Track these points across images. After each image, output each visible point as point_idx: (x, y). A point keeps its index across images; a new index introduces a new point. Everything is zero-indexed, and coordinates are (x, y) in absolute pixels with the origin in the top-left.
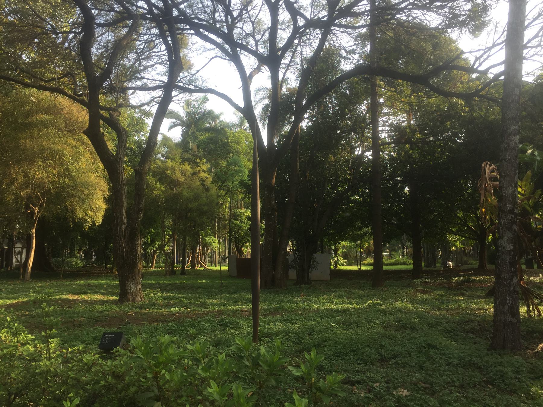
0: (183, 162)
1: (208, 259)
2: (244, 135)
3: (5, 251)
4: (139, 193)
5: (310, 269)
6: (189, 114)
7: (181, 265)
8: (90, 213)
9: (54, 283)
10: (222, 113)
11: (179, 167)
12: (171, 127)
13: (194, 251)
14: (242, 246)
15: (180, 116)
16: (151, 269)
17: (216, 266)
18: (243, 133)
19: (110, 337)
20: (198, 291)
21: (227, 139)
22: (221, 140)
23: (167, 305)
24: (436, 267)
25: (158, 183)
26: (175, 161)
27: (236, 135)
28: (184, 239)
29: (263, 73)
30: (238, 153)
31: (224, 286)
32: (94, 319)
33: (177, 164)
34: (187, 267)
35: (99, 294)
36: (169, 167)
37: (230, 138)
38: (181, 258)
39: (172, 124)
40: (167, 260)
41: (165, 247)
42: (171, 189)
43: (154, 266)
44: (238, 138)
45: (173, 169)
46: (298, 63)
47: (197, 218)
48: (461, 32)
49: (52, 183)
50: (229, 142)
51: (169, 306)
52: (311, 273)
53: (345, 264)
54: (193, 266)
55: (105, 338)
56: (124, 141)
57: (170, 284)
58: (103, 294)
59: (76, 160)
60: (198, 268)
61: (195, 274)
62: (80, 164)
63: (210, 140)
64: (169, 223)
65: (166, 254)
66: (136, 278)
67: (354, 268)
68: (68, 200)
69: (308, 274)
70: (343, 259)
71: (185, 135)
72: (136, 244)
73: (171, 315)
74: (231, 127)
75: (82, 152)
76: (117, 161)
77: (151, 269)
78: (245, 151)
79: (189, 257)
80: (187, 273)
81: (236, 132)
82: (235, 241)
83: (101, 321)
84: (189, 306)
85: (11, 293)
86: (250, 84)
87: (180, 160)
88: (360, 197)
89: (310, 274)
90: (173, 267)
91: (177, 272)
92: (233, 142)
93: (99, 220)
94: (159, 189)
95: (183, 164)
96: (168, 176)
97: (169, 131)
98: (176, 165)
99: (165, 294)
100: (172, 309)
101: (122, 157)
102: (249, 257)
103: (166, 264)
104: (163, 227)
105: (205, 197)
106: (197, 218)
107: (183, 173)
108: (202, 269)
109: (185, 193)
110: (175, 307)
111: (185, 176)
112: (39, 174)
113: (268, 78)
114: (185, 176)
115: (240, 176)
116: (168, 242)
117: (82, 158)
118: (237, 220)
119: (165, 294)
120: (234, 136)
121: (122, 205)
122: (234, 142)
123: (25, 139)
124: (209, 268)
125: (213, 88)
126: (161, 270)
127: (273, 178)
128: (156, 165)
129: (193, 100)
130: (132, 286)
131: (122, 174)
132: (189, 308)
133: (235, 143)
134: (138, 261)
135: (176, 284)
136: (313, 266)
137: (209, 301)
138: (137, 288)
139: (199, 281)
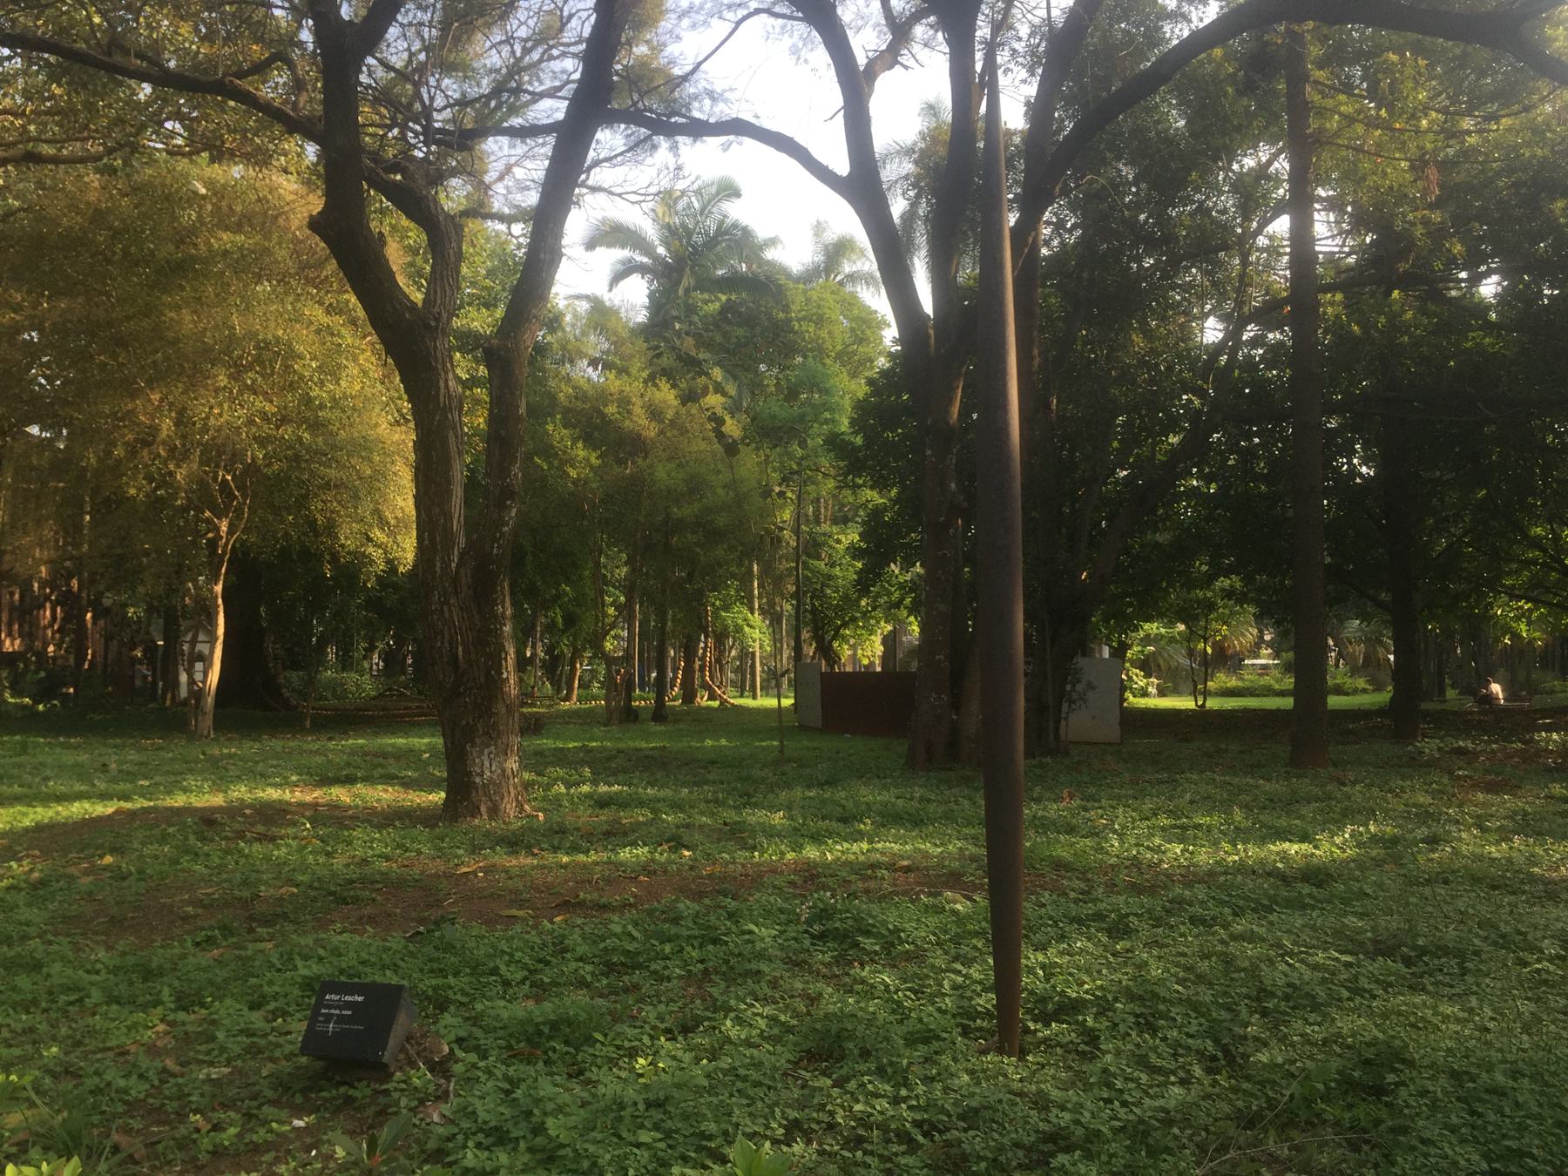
1: (731, 675)
2: (838, 298)
3: (160, 652)
4: (503, 433)
5: (1065, 706)
6: (671, 233)
7: (652, 695)
8: (378, 535)
9: (277, 744)
10: (772, 242)
11: (642, 396)
12: (617, 278)
13: (689, 652)
14: (834, 638)
15: (645, 239)
16: (566, 705)
18: (833, 293)
19: (348, 1005)
20: (710, 777)
21: (786, 309)
23: (608, 834)
26: (629, 374)
27: (815, 298)
28: (662, 620)
29: (906, 67)
30: (820, 351)
31: (789, 761)
32: (331, 893)
33: (638, 385)
34: (670, 700)
35: (393, 785)
36: (611, 395)
38: (654, 675)
39: (620, 267)
42: (621, 462)
43: (575, 698)
44: (819, 307)
45: (624, 402)
46: (1021, 34)
47: (698, 550)
49: (262, 442)
50: (790, 320)
51: (616, 835)
52: (1066, 719)
54: (689, 696)
55: (329, 1007)
56: (453, 259)
57: (620, 751)
58: (407, 784)
59: (330, 370)
60: (703, 700)
62: (343, 383)
66: (499, 735)
67: (1186, 703)
68: (316, 495)
69: (1058, 722)
70: (1145, 677)
71: (658, 305)
72: (496, 616)
73: (619, 876)
74: (810, 276)
75: (348, 345)
76: (427, 327)
77: (566, 705)
78: (839, 348)
79: (675, 671)
80: (671, 718)
82: (814, 621)
83: (356, 900)
84: (686, 840)
85: (130, 776)
86: (870, 96)
87: (645, 374)
88: (1208, 479)
89: (1063, 723)
90: (629, 699)
92: (804, 319)
93: (407, 550)
94: (582, 460)
95: (655, 385)
97: (611, 290)
99: (603, 789)
100: (625, 854)
101: (445, 315)
102: (879, 669)
104: (601, 582)
105: (724, 487)
106: (698, 550)
107: (655, 413)
108: (716, 704)
109: (661, 473)
110: (634, 844)
111: (661, 421)
112: (221, 415)
113: (918, 110)
114: (661, 421)
115: (826, 422)
116: (613, 626)
117: (351, 365)
118: (819, 558)
119: (603, 789)
120: (808, 300)
121: (449, 483)
123: (178, 308)
126: (597, 706)
127: (950, 401)
128: (574, 388)
129: (683, 192)
130: (487, 764)
131: (446, 373)
132: (688, 848)
133: (811, 321)
134: (505, 676)
135: (641, 749)
136: (1075, 696)
137: (755, 817)
138: (504, 771)
139: (709, 743)
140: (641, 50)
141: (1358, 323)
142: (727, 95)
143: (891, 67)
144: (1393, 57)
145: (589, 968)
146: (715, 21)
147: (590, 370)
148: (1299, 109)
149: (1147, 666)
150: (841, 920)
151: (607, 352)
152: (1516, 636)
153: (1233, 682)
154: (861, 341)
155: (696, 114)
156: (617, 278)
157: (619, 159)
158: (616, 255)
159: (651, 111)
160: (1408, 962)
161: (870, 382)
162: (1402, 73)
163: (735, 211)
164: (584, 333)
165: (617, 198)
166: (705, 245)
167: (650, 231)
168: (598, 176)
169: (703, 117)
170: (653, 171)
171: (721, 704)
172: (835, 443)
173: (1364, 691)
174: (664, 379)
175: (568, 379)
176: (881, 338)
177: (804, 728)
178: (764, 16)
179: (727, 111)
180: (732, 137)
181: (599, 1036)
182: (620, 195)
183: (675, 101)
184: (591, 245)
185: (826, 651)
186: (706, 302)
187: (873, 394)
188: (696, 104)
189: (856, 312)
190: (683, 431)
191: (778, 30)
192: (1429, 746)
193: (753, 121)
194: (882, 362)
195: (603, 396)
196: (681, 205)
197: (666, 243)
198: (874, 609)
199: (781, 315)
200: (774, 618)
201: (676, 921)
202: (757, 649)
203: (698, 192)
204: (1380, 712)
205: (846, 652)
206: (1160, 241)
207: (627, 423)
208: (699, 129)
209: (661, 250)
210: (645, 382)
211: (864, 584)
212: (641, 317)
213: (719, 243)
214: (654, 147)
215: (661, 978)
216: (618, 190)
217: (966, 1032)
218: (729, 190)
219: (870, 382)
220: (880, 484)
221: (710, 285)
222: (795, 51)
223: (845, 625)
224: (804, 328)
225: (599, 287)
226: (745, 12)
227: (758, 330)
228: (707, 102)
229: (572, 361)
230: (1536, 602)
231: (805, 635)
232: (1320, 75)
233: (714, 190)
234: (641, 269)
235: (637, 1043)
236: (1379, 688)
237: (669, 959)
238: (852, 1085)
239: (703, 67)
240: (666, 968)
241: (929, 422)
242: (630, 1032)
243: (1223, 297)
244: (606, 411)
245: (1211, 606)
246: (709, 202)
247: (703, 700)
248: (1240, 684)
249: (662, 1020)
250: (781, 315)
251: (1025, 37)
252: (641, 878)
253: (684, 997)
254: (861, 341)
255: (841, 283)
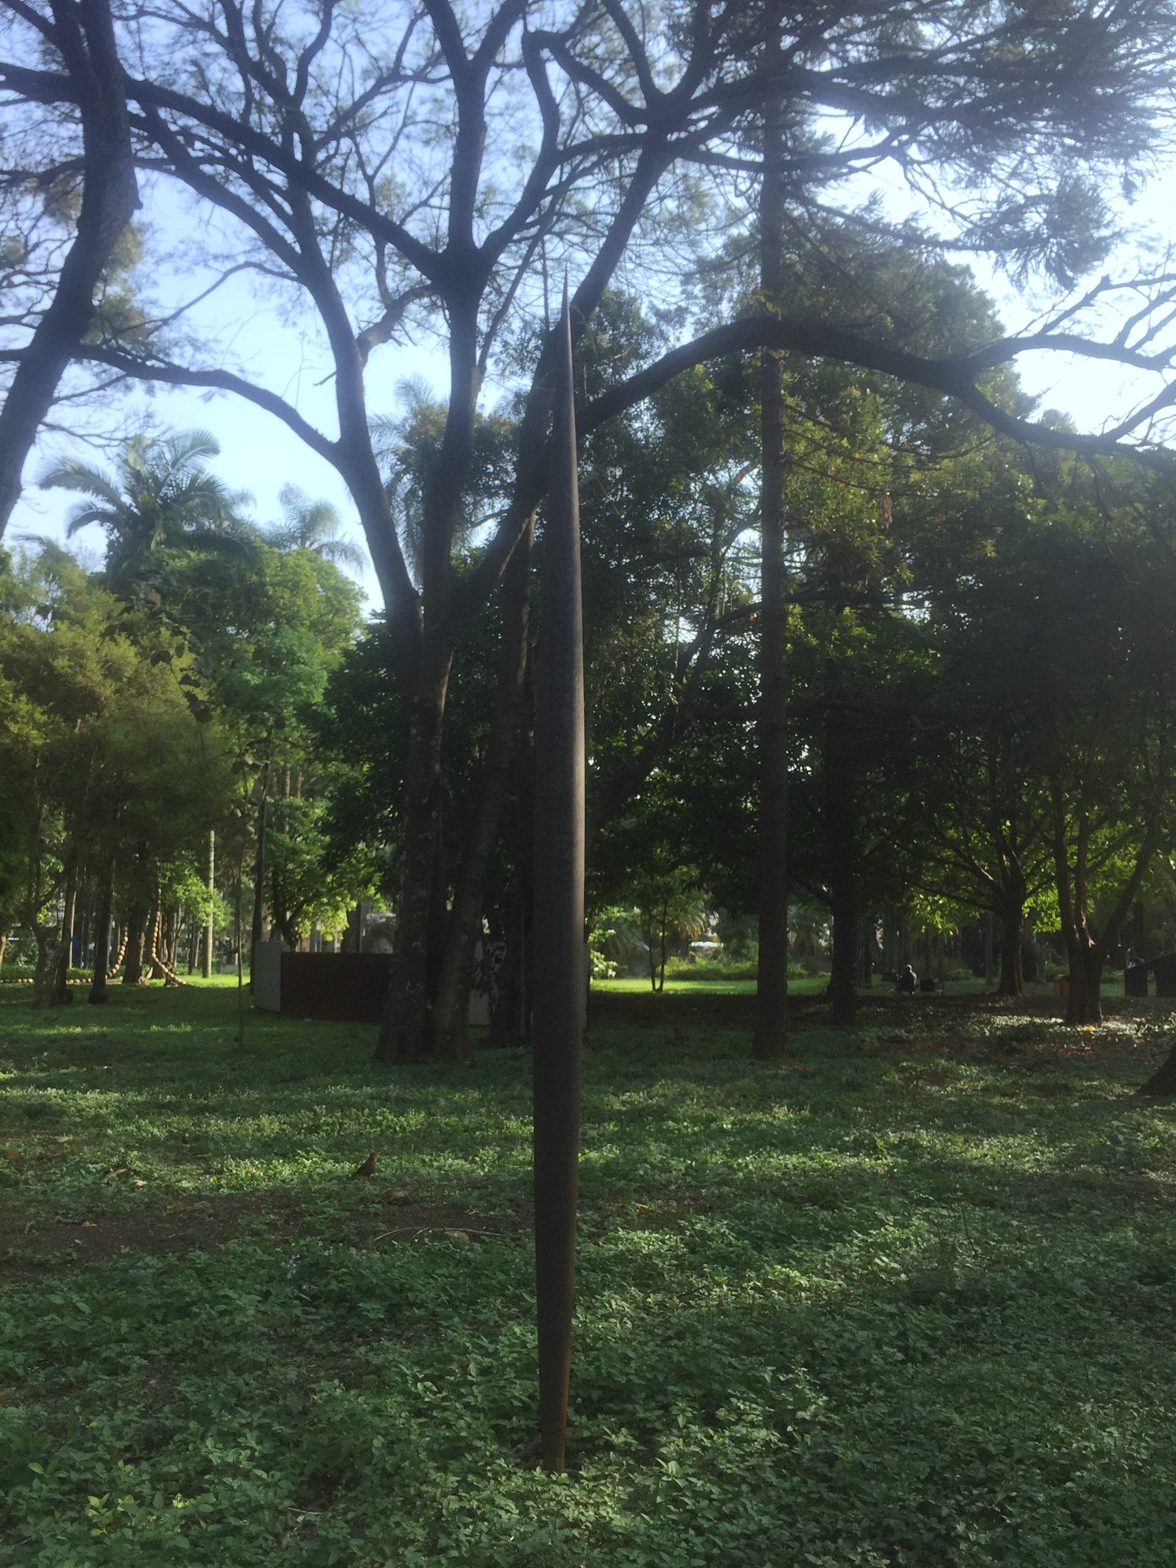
0: (109, 633)
2: (315, 566)
6: (139, 482)
10: (244, 498)
12: (76, 524)
15: (108, 485)
17: (205, 975)
21: (260, 573)
22: (242, 579)
24: (870, 987)
25: (23, 698)
27: (291, 564)
29: (400, 343)
30: (292, 619)
33: (94, 638)
37: (268, 571)
40: (43, 956)
41: (39, 910)
44: (295, 573)
48: (1024, 267)
50: (263, 584)
53: (611, 972)
60: (147, 979)
61: (138, 1002)
63: (200, 574)
64: (58, 833)
65: (44, 934)
67: (642, 985)
71: (117, 555)
74: (278, 541)
81: (289, 554)
82: (275, 896)
87: (102, 628)
90: (64, 976)
91: (78, 996)
92: (278, 584)
95: (115, 640)
96: (60, 675)
97: (69, 536)
98: (89, 641)
103: (41, 965)
107: (112, 670)
108: (160, 982)
116: (49, 897)
120: (283, 566)
122: (282, 584)
124: (184, 980)
125: (232, 370)
129: (154, 443)
140: (114, 290)
141: (815, 636)
142: (212, 345)
143: (384, 341)
144: (856, 393)
145: (20, 1357)
146: (199, 270)
147: (38, 618)
148: (772, 431)
149: (607, 949)
150: (336, 1277)
151: (61, 599)
152: (932, 927)
153: (684, 966)
154: (338, 611)
155: (176, 361)
156: (76, 524)
157: (83, 398)
158: (79, 497)
159: (124, 350)
160: (949, 1311)
161: (346, 653)
162: (863, 408)
163: (213, 468)
164: (34, 579)
165: (79, 440)
166: (176, 499)
167: (115, 477)
168: (54, 414)
169: (185, 365)
170: (120, 416)
171: (168, 982)
172: (305, 713)
173: (801, 976)
174: (124, 634)
175: (13, 627)
176: (358, 610)
177: (261, 1011)
178: (251, 271)
179: (211, 362)
180: (214, 389)
181: (36, 1468)
182: (81, 437)
183: (152, 343)
184: (46, 483)
185: (285, 928)
186: (173, 557)
187: (348, 666)
188: (177, 351)
189: (333, 582)
190: (142, 691)
191: (266, 288)
192: (870, 1035)
193: (238, 375)
194: (359, 635)
195: (51, 648)
196: (151, 453)
197: (132, 492)
198: (340, 885)
199: (254, 578)
200: (234, 895)
201: (131, 1285)
202: (211, 924)
203: (171, 443)
204: (818, 999)
205: (305, 929)
206: (643, 538)
207: (80, 678)
208: (177, 376)
209: (126, 499)
210: (103, 635)
211: (329, 863)
212: (100, 567)
213: (191, 499)
214: (128, 388)
215: (114, 1369)
216: (81, 432)
217: (500, 1434)
218: (206, 445)
219: (346, 653)
220: (352, 759)
221: (176, 539)
222: (283, 313)
223: (308, 901)
224: (279, 594)
225: (55, 530)
226: (234, 265)
227: (229, 592)
228: (189, 350)
229: (17, 608)
230: (950, 897)
231: (265, 911)
232: (790, 401)
233: (188, 444)
234: (103, 517)
235: (89, 1476)
236: (813, 973)
237: (125, 1340)
238: (375, 1530)
239: (187, 313)
240: (121, 1354)
241: (416, 700)
242: (78, 1457)
243: (692, 600)
244: (55, 663)
245: (669, 891)
246: (183, 454)
247: (147, 979)
248: (691, 967)
249: (120, 1438)
250: (254, 578)
251: (517, 331)
252: (87, 1224)
253: (145, 1396)
254: (338, 611)
255: (319, 551)
